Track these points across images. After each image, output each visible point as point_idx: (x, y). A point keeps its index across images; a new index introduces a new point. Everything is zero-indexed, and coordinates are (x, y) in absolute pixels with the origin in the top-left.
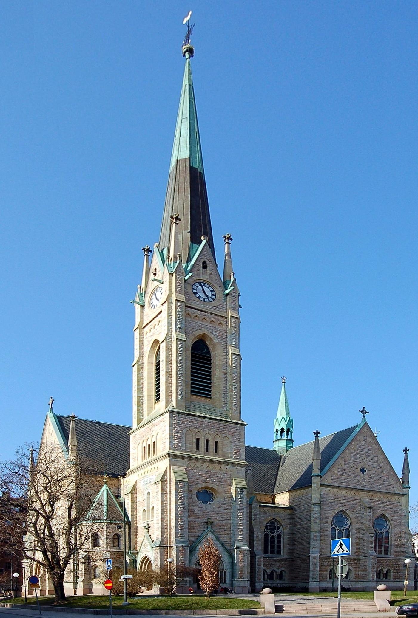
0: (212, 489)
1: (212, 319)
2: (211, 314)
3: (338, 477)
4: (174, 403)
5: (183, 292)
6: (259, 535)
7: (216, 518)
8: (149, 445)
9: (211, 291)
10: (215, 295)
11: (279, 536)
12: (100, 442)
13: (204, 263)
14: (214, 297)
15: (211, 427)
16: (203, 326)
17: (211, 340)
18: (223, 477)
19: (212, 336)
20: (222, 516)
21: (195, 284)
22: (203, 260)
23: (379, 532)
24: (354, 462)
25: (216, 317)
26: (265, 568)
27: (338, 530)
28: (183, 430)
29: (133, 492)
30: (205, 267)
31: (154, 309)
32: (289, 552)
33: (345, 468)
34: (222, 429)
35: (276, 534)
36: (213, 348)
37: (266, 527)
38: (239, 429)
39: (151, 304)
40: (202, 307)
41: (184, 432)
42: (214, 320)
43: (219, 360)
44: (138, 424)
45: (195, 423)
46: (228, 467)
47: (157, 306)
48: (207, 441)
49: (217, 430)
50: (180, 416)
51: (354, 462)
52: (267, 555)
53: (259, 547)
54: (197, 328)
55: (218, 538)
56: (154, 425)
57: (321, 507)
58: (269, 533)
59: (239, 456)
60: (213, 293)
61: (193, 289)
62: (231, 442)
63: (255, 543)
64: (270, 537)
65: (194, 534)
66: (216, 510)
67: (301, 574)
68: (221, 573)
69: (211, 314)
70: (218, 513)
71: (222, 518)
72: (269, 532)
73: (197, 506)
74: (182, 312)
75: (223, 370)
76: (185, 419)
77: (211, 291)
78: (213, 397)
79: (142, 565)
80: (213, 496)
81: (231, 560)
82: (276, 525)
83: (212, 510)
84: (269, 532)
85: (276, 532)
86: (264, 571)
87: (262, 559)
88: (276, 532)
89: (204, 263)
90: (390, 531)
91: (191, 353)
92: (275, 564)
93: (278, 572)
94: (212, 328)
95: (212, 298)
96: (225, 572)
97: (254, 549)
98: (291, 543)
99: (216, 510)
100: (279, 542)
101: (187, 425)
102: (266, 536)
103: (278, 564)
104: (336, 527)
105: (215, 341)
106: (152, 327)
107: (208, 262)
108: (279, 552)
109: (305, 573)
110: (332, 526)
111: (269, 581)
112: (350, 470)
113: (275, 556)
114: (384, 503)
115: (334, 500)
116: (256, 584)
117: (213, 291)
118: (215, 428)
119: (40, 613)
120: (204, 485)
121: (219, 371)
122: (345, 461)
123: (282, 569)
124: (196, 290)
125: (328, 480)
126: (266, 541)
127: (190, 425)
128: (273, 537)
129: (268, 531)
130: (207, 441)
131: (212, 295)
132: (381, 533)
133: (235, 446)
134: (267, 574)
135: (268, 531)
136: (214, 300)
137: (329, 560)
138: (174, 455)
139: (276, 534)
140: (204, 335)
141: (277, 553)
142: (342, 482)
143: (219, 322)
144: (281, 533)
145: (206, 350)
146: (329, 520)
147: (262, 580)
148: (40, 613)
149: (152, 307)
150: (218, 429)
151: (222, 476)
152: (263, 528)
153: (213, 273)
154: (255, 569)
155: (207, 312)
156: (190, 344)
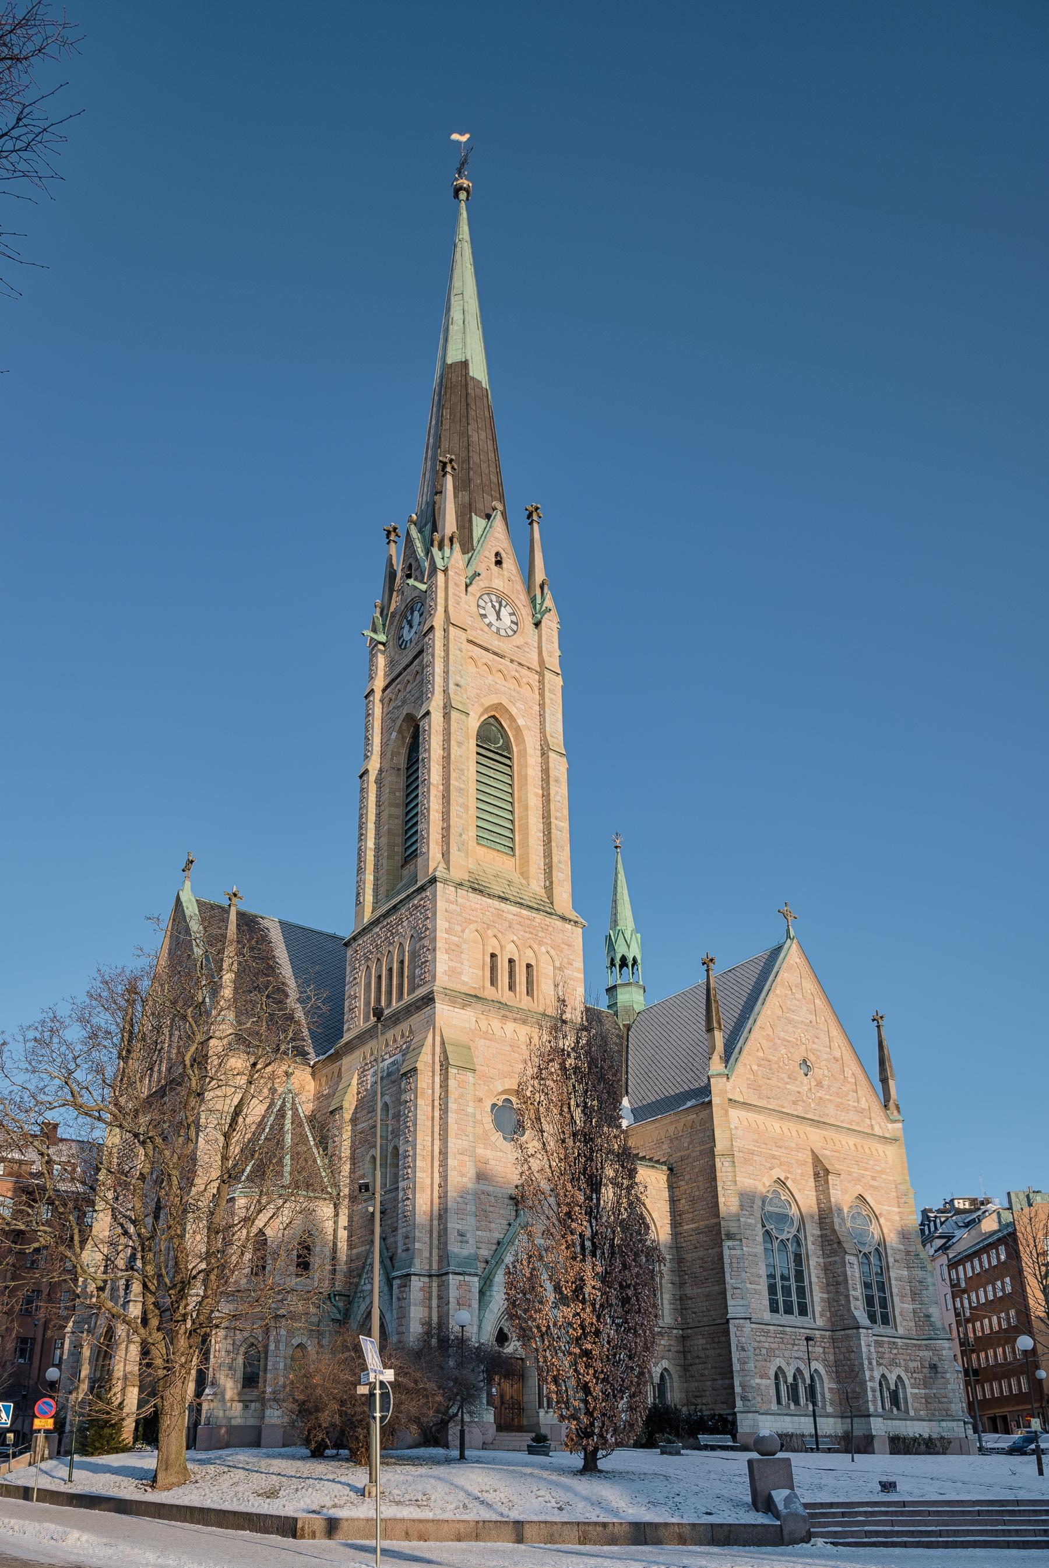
9: (512, 622)
17: (512, 718)
21: (483, 597)
23: (777, 1238)
25: (519, 668)
30: (499, 563)
31: (405, 648)
39: (400, 639)
40: (495, 644)
47: (411, 642)
48: (511, 987)
49: (530, 935)
60: (514, 618)
61: (478, 606)
67: (709, 1383)
77: (510, 614)
85: (786, 1232)
89: (497, 554)
90: (802, 1236)
107: (503, 555)
109: (720, 1382)
110: (764, 1226)
114: (857, 1163)
119: (70, 1475)
122: (768, 1038)
124: (484, 608)
130: (511, 987)
132: (782, 1241)
140: (499, 706)
145: (501, 741)
148: (70, 1475)
149: (400, 646)
155: (502, 657)
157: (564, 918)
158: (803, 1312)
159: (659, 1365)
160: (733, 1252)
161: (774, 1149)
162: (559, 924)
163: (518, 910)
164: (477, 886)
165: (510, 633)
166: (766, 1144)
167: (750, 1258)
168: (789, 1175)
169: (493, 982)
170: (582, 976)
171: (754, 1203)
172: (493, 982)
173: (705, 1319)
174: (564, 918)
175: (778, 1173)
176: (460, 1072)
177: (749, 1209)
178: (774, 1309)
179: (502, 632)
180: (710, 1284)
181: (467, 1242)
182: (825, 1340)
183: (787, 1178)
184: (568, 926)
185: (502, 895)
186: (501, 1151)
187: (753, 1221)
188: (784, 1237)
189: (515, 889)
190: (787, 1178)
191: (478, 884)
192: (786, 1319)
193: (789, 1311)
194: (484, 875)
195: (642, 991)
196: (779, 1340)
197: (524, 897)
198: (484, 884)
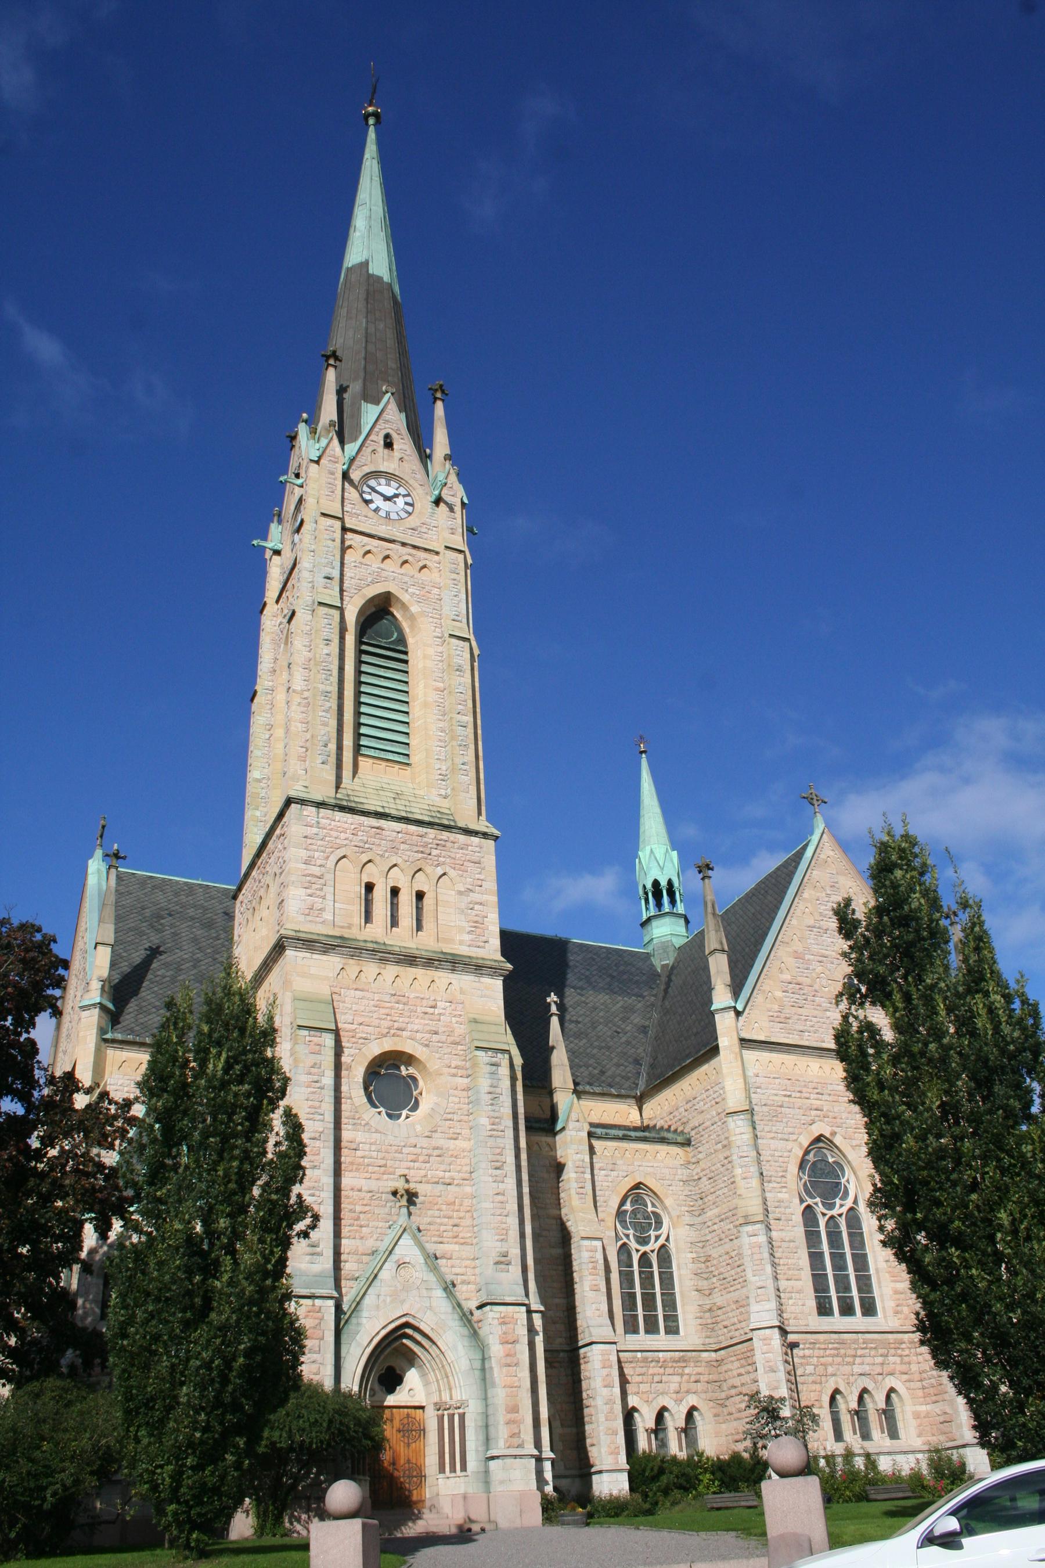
1: (405, 558)
2: (404, 544)
3: (788, 1011)
7: (423, 1172)
10: (412, 505)
12: (195, 940)
13: (387, 436)
14: (410, 509)
15: (403, 846)
16: (384, 574)
17: (404, 607)
18: (440, 1014)
19: (405, 597)
20: (443, 1167)
22: (383, 433)
24: (821, 959)
27: (824, 1215)
28: (328, 857)
30: (389, 444)
32: (703, 1321)
33: (800, 979)
34: (434, 852)
35: (653, 1246)
36: (412, 627)
38: (478, 849)
40: (382, 530)
42: (410, 558)
43: (425, 657)
45: (360, 833)
46: (454, 978)
49: (420, 855)
50: (321, 815)
51: (821, 959)
54: (370, 580)
55: (432, 1259)
57: (754, 1128)
59: (484, 939)
62: (460, 893)
65: (358, 1242)
66: (424, 1142)
68: (451, 1417)
69: (404, 544)
70: (430, 1152)
71: (441, 1174)
72: (631, 1237)
73: (367, 1127)
75: (434, 683)
76: (333, 823)
78: (413, 760)
80: (417, 1087)
81: (479, 1356)
82: (650, 1209)
83: (413, 1141)
84: (631, 1237)
88: (653, 1239)
89: (387, 436)
92: (664, 1378)
94: (406, 579)
95: (407, 512)
96: (462, 1417)
98: (704, 1284)
100: (667, 1280)
101: (338, 841)
104: (816, 1204)
105: (414, 609)
107: (394, 435)
108: (672, 1329)
110: (802, 1201)
112: (816, 987)
115: (789, 1096)
117: (408, 495)
118: (416, 849)
121: (425, 687)
122: (797, 956)
123: (692, 1400)
125: (758, 1028)
127: (345, 842)
128: (644, 1260)
129: (627, 1236)
130: (394, 922)
131: (406, 503)
133: (471, 906)
135: (627, 1236)
136: (410, 514)
137: (817, 1352)
139: (653, 1246)
141: (647, 1332)
142: (801, 1028)
143: (421, 564)
144: (667, 1239)
145: (395, 635)
146: (789, 1176)
150: (422, 852)
151: (437, 1011)
153: (406, 457)
157: (468, 832)
158: (869, 1309)
159: (684, 1402)
160: (754, 1239)
161: (812, 1096)
162: (462, 838)
163: (404, 826)
164: (345, 803)
165: (403, 515)
166: (800, 1092)
167: (784, 1245)
168: (837, 1130)
169: (368, 917)
170: (495, 899)
171: (786, 1171)
172: (368, 917)
173: (737, 1333)
174: (468, 832)
175: (817, 1130)
176: (312, 1033)
177: (779, 1180)
178: (824, 1309)
179: (393, 516)
180: (739, 1286)
181: (320, 1254)
182: (903, 1346)
183: (834, 1134)
184: (475, 840)
185: (380, 810)
186: (377, 1131)
187: (786, 1196)
188: (835, 1212)
189: (403, 802)
190: (834, 1134)
191: (349, 801)
192: (837, 1321)
193: (847, 1310)
194: (363, 789)
195: (682, 921)
196: (832, 1352)
197: (413, 810)
198: (356, 799)
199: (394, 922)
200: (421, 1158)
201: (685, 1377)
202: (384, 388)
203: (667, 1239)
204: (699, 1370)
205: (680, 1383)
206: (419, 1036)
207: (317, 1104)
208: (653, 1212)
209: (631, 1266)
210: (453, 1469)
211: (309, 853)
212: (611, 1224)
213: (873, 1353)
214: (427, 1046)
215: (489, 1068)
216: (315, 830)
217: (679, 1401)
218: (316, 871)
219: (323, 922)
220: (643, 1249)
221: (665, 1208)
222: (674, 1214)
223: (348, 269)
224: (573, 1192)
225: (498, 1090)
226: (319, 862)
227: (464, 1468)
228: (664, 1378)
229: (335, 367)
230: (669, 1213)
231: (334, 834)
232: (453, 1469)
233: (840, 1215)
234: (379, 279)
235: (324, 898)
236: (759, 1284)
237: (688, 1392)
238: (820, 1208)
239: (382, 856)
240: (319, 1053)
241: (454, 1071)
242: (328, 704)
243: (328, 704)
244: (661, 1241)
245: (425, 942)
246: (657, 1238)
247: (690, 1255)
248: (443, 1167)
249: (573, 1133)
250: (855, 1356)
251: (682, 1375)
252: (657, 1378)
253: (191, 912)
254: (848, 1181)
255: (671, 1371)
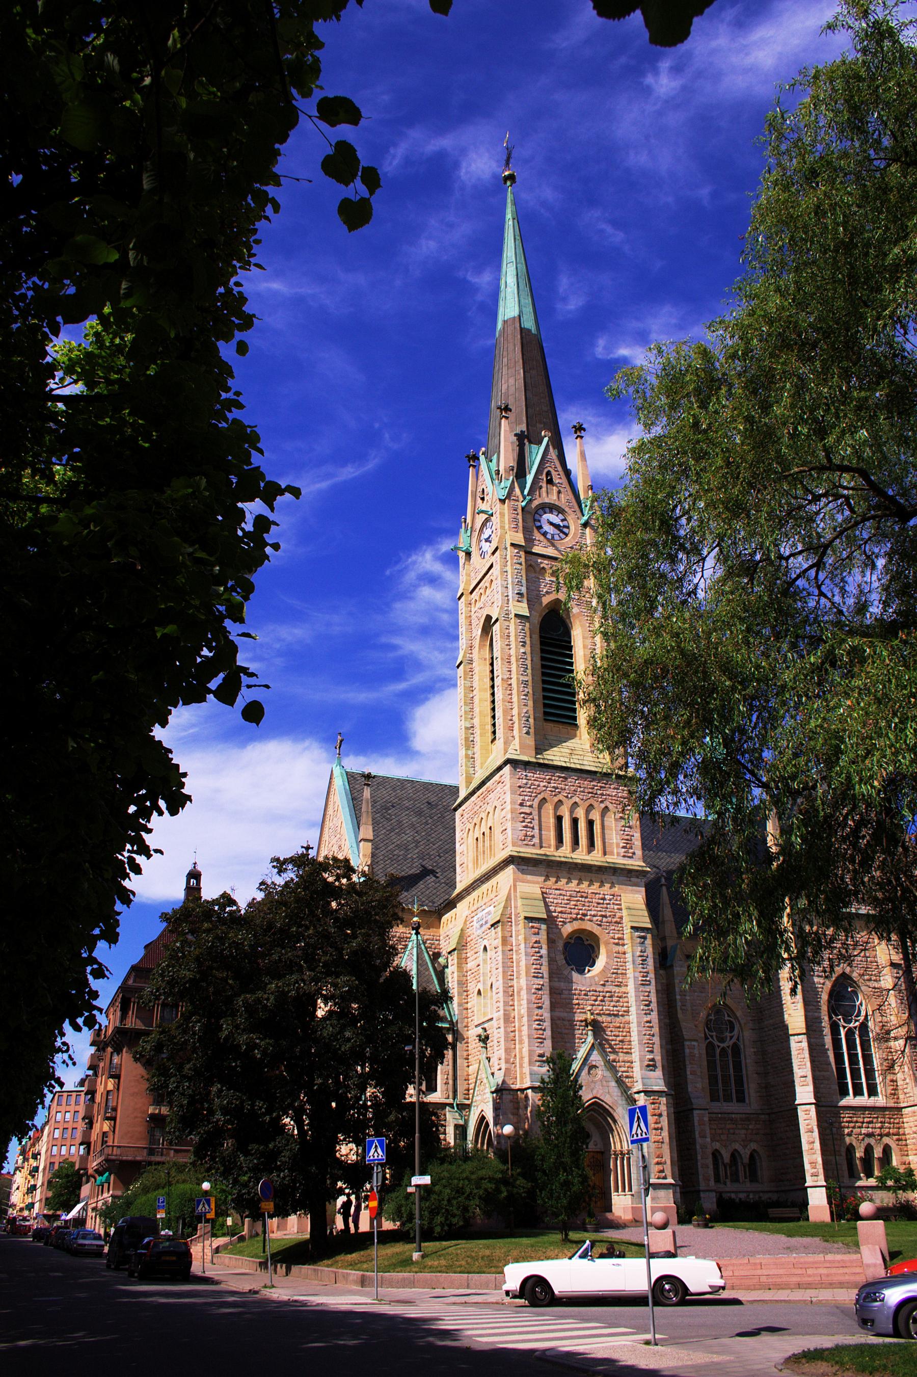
0: (591, 934)
4: (516, 744)
5: (521, 528)
6: (695, 1049)
8: (484, 834)
11: (736, 1049)
26: (717, 1145)
27: (844, 1027)
29: (461, 946)
34: (599, 792)
37: (708, 1023)
41: (536, 804)
44: (467, 787)
52: (717, 1107)
53: (697, 1084)
56: (489, 791)
58: (716, 1043)
63: (688, 1073)
64: (718, 1051)
74: (521, 564)
79: (476, 1141)
86: (716, 1155)
87: (706, 1119)
91: (541, 637)
92: (737, 1131)
93: (745, 1153)
97: (690, 1090)
99: (600, 989)
100: (738, 1067)
102: (710, 1047)
103: (743, 1131)
106: (482, 591)
111: (728, 1183)
113: (733, 1107)
116: (702, 1195)
120: (576, 925)
123: (753, 1146)
126: (711, 1065)
129: (712, 1037)
130: (576, 842)
134: (723, 1163)
135: (712, 1037)
138: (520, 857)
139: (728, 1043)
144: (738, 1039)
147: (712, 1183)
152: (701, 1027)
154: (696, 1149)
156: (537, 620)
188: (852, 1025)
197: (585, 763)
199: (576, 842)
200: (599, 998)
201: (750, 1131)
202: (543, 433)
203: (738, 1039)
204: (758, 1126)
205: (746, 1134)
206: (595, 919)
207: (538, 966)
208: (729, 1021)
209: (715, 1056)
210: (624, 1190)
211: (522, 798)
212: (701, 1029)
213: (875, 1120)
214: (600, 925)
215: (639, 940)
216: (525, 781)
217: (745, 1147)
218: (527, 810)
219: (534, 845)
220: (722, 1045)
221: (736, 1018)
222: (742, 1022)
223: (505, 322)
224: (678, 1008)
225: (645, 954)
226: (528, 803)
227: (630, 1190)
228: (737, 1131)
229: (507, 418)
230: (739, 1021)
231: (537, 783)
232: (624, 1190)
233: (855, 1028)
234: (529, 331)
235: (533, 828)
236: (802, 1074)
237: (751, 1141)
238: (842, 1022)
239: (567, 797)
240: (538, 934)
241: (616, 941)
242: (526, 690)
243: (526, 690)
244: (734, 1040)
245: (596, 858)
246: (731, 1038)
247: (752, 1050)
248: (612, 1004)
249: (678, 969)
250: (863, 1123)
251: (747, 1129)
252: (731, 1131)
253: (407, 803)
254: (861, 1004)
255: (740, 1127)
